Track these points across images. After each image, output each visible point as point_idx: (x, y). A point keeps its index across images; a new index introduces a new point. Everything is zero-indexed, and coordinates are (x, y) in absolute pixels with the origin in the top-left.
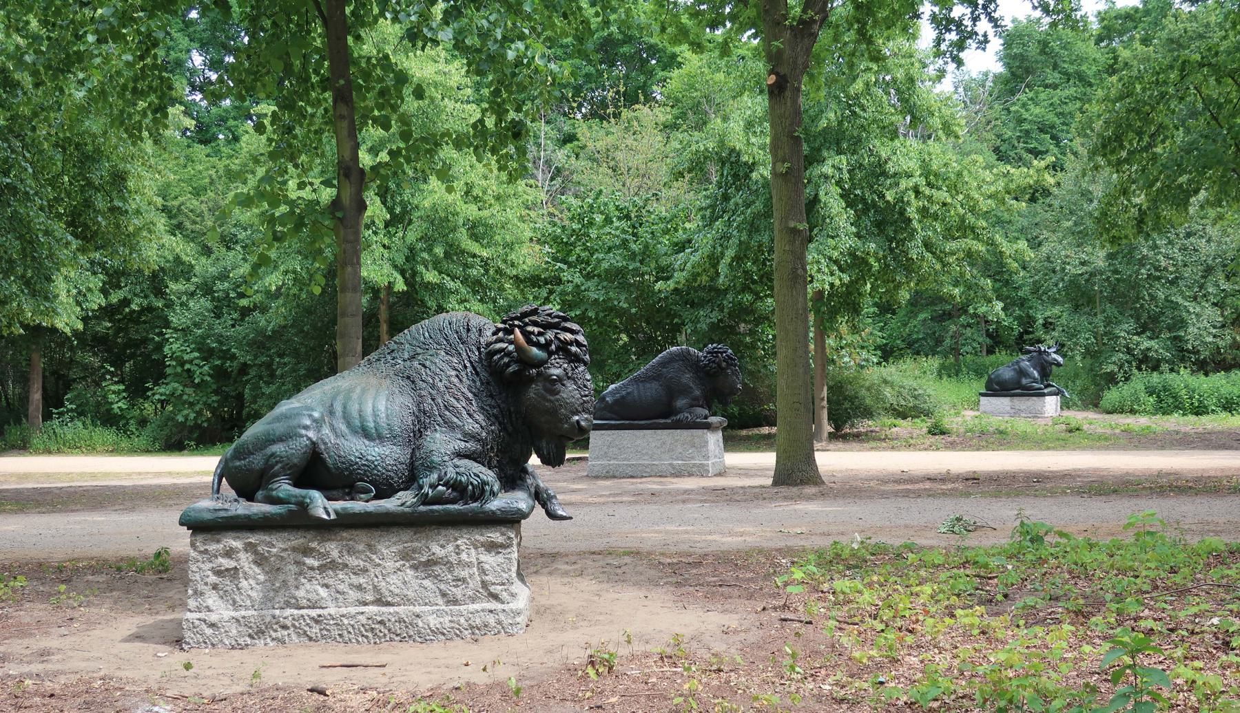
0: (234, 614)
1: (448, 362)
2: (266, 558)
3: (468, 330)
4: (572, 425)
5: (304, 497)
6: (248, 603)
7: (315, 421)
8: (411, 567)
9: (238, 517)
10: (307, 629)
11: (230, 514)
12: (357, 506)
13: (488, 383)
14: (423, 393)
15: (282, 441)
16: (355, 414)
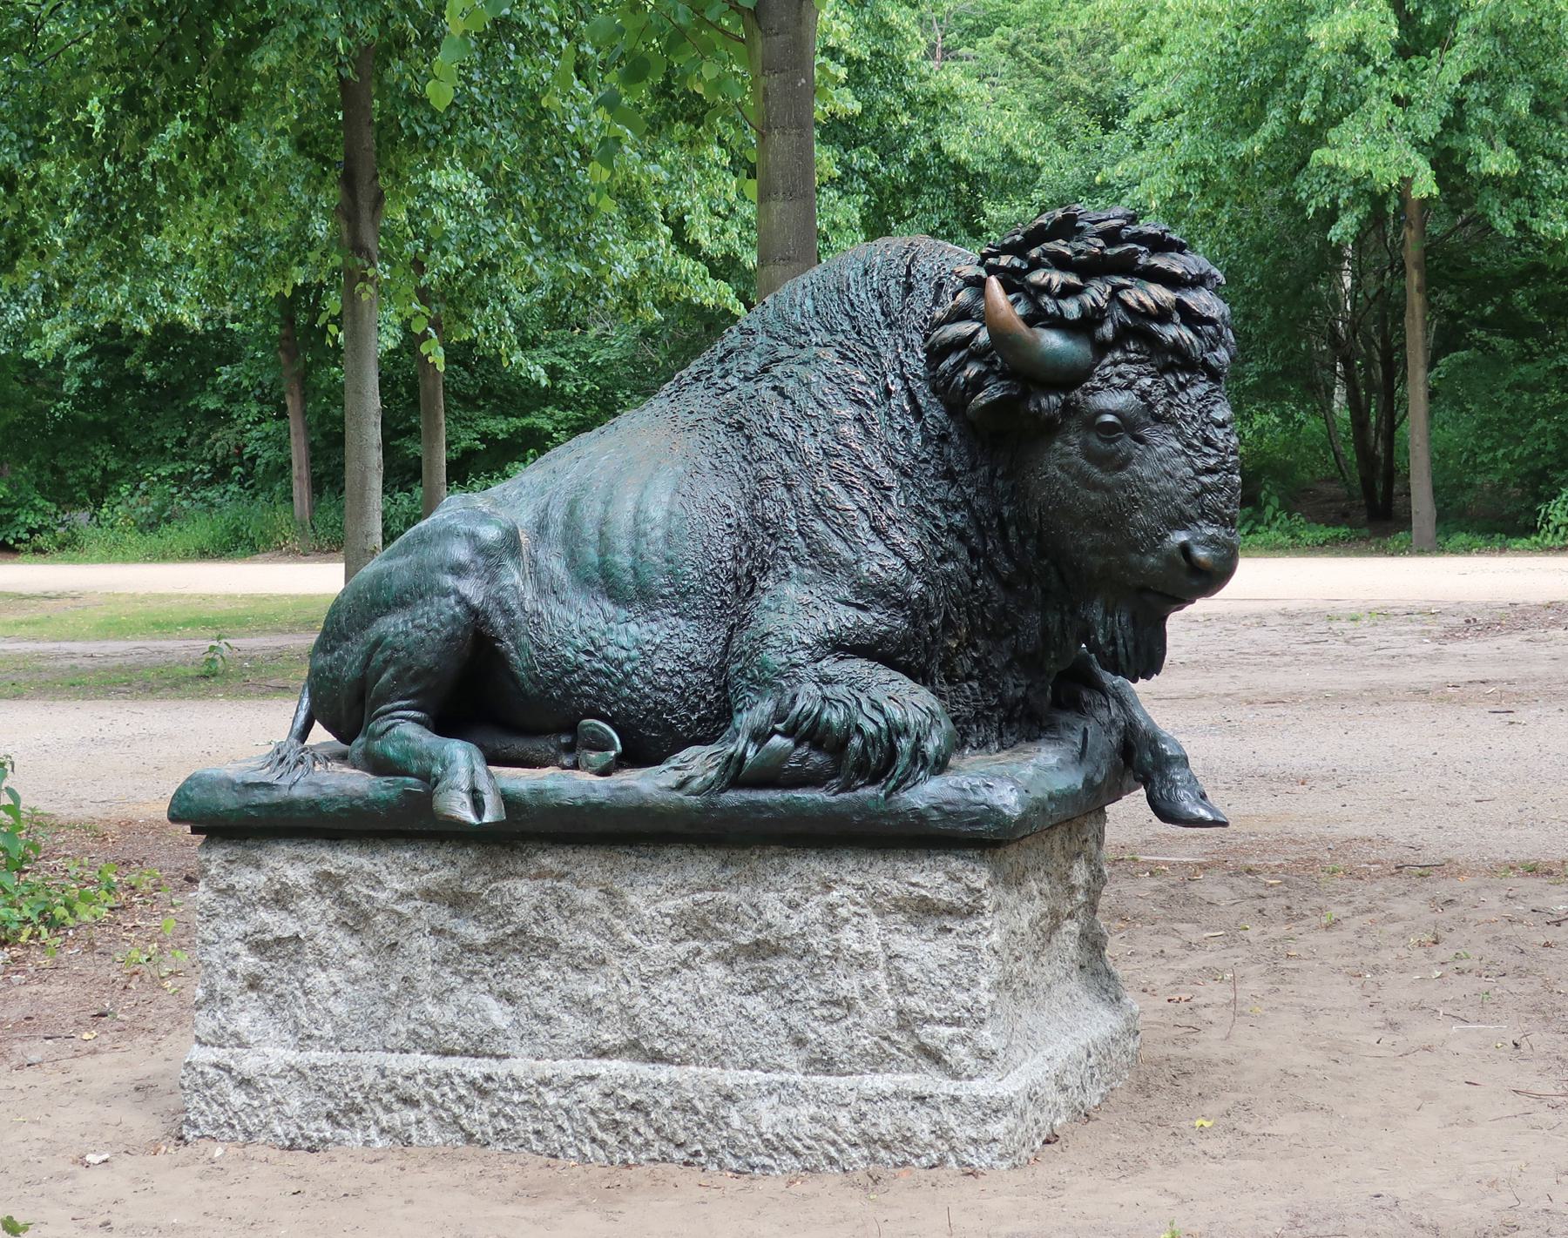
0: (292, 1056)
1: (839, 381)
2: (366, 917)
3: (909, 289)
4: (1169, 560)
6: (328, 1030)
7: (483, 550)
8: (717, 957)
9: (291, 805)
10: (459, 1109)
11: (276, 796)
13: (943, 438)
15: (403, 604)
16: (590, 531)
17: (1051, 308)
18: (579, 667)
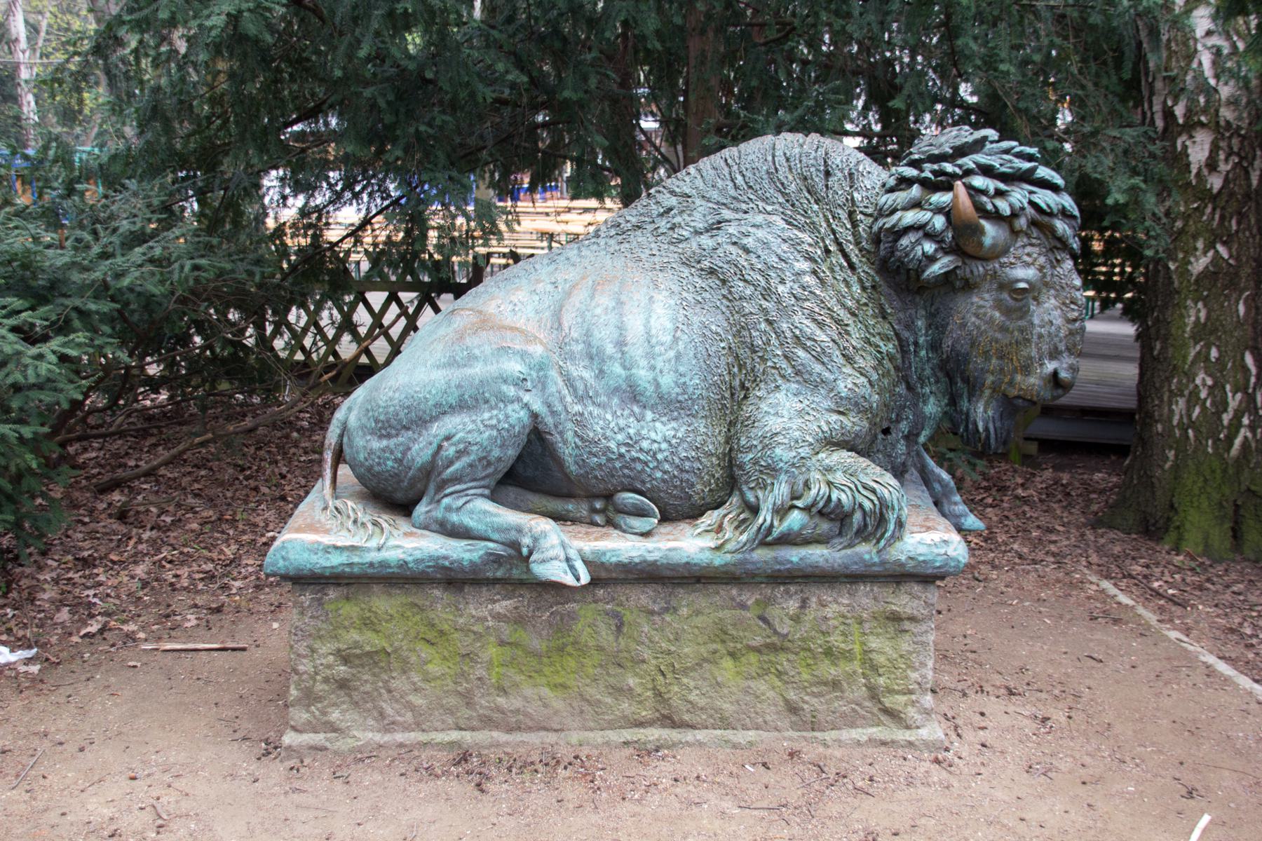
1: (795, 244)
3: (828, 174)
5: (519, 530)
9: (384, 564)
12: (622, 546)
14: (748, 307)
17: (989, 207)
18: (621, 456)
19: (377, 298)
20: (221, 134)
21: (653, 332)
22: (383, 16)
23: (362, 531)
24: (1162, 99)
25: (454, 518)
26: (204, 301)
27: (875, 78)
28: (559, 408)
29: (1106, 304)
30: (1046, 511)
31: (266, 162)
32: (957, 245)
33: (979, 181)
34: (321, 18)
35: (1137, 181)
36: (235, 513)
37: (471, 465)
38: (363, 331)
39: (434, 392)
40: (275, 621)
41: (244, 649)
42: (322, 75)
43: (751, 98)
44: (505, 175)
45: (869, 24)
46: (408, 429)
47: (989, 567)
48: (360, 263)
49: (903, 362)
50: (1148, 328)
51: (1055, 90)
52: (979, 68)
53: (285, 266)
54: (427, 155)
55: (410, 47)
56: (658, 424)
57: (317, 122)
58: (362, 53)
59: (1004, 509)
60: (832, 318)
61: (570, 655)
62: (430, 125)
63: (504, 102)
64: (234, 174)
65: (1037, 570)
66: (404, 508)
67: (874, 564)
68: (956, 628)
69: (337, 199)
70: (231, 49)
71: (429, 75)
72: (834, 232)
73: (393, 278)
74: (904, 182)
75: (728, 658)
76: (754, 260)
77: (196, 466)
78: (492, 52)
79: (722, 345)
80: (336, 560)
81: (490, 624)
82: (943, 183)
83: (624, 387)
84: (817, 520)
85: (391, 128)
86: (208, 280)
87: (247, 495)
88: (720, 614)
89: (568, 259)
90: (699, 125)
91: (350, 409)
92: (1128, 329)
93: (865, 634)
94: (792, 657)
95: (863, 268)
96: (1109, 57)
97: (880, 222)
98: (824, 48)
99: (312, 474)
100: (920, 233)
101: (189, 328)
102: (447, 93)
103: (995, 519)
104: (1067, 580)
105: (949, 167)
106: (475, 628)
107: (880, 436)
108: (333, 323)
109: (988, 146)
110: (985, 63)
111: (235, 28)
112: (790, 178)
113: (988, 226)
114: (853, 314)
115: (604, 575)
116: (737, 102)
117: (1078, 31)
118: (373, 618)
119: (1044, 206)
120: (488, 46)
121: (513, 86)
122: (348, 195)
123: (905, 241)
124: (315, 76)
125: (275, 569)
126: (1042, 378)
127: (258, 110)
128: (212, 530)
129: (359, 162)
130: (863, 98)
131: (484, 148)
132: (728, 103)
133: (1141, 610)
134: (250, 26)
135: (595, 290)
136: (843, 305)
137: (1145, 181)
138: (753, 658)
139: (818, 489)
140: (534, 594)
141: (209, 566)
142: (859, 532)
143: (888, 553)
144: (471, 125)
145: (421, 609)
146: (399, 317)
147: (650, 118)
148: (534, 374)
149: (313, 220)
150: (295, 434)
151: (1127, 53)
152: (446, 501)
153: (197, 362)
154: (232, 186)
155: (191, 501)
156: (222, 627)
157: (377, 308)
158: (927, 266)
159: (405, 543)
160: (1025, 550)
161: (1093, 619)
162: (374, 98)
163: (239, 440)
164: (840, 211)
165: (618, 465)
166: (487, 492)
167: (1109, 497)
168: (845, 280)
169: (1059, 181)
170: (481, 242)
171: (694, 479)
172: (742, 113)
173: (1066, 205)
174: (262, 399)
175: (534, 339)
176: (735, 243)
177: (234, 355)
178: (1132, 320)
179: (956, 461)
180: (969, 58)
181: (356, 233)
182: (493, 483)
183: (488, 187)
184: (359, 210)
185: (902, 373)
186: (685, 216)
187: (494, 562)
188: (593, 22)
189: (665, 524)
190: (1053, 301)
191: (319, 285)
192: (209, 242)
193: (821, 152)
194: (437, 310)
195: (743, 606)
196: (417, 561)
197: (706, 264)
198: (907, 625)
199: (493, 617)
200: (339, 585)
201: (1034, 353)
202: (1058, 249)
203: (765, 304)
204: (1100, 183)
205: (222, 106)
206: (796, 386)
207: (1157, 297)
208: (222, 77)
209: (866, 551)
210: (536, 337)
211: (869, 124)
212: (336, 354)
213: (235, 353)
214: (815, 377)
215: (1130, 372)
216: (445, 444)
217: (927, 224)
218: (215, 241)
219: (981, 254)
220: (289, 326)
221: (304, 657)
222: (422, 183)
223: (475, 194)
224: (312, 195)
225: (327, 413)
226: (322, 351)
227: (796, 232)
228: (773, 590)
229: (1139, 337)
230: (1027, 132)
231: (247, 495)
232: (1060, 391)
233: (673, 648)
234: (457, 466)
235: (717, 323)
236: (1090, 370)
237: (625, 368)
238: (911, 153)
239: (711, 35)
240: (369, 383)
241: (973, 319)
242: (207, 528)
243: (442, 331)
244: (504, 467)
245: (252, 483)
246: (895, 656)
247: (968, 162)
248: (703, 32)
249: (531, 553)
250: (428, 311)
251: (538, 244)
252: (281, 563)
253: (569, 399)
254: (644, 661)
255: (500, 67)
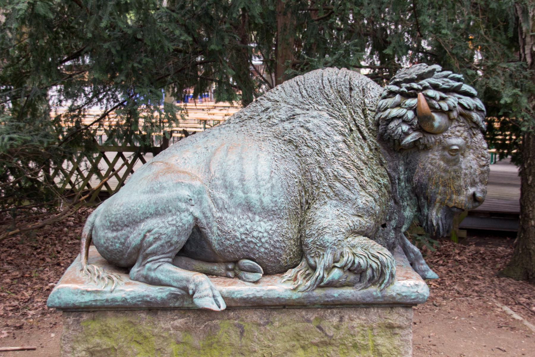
1: (334, 126)
3: (351, 89)
9: (114, 300)
12: (243, 289)
14: (309, 160)
17: (437, 106)
18: (242, 240)
19: (111, 155)
20: (25, 66)
21: (259, 174)
22: (114, 5)
23: (102, 282)
24: (530, 47)
25: (152, 274)
26: (16, 157)
27: (376, 38)
28: (209, 214)
29: (502, 156)
30: (472, 268)
31: (50, 82)
32: (420, 126)
33: (431, 93)
34: (80, 5)
35: (517, 91)
36: (31, 273)
37: (162, 246)
38: (103, 173)
39: (142, 206)
40: (53, 332)
41: (34, 349)
42: (81, 35)
43: (311, 48)
44: (180, 89)
45: (373, 9)
46: (128, 226)
47: (441, 298)
48: (102, 136)
49: (392, 189)
50: (525, 169)
51: (472, 43)
52: (431, 32)
53: (61, 137)
54: (138, 79)
55: (129, 22)
56: (262, 223)
57: (78, 60)
58: (103, 25)
59: (449, 267)
60: (354, 165)
61: (215, 348)
62: (139, 63)
63: (180, 51)
64: (32, 88)
65: (468, 300)
66: (126, 269)
67: (379, 298)
68: (425, 332)
69: (89, 102)
70: (30, 21)
71: (139, 36)
72: (355, 120)
73: (120, 145)
74: (392, 94)
75: (301, 349)
76: (313, 135)
77: (9, 247)
78: (173, 25)
79: (296, 180)
80: (87, 298)
81: (172, 332)
82: (412, 94)
83: (244, 203)
84: (347, 273)
85: (120, 63)
86: (18, 146)
87: (38, 263)
88: (296, 325)
89: (214, 135)
90: (283, 63)
91: (96, 216)
92: (514, 169)
93: (374, 336)
94: (335, 348)
95: (371, 139)
96: (501, 25)
97: (379, 115)
98: (349, 22)
99: (75, 251)
100: (401, 120)
101: (7, 172)
102: (149, 46)
103: (444, 272)
104: (484, 305)
105: (415, 85)
106: (164, 335)
107: (381, 228)
108: (87, 169)
109: (436, 74)
110: (435, 29)
111: (33, 9)
112: (331, 91)
113: (436, 116)
114: (365, 164)
115: (233, 304)
116: (303, 50)
117: (484, 11)
118: (107, 330)
119: (466, 106)
120: (170, 21)
121: (184, 42)
122: (95, 100)
123: (392, 125)
124: (77, 36)
125: (53, 304)
126: (467, 197)
127: (46, 54)
128: (18, 283)
129: (101, 82)
130: (370, 48)
131: (169, 75)
132: (299, 51)
133: (526, 323)
134: (41, 9)
135: (228, 151)
136: (360, 159)
137: (521, 91)
138: (314, 349)
139: (348, 258)
140: (196, 316)
141: (16, 303)
142: (370, 280)
143: (386, 291)
144: (162, 63)
145: (134, 325)
146: (123, 165)
147: (257, 59)
148: (196, 197)
149: (76, 113)
150: (66, 229)
151: (511, 23)
152: (148, 265)
153: (11, 190)
154: (31, 95)
155: (6, 266)
156: (22, 337)
157: (111, 160)
158: (404, 138)
159: (126, 288)
160: (461, 289)
161: (500, 327)
162: (109, 48)
163: (35, 232)
164: (358, 109)
165: (241, 245)
166: (170, 260)
167: (506, 260)
168: (361, 145)
169: (474, 92)
170: (167, 125)
171: (281, 252)
172: (306, 57)
173: (478, 104)
174: (48, 210)
175: (195, 178)
176: (302, 126)
177: (32, 187)
178: (516, 165)
179: (422, 241)
180: (426, 27)
181: (100, 120)
182: (174, 255)
183: (171, 96)
184: (102, 108)
185: (392, 194)
186: (276, 112)
187: (174, 298)
188: (226, 9)
189: (266, 277)
190: (472, 156)
191: (80, 148)
192: (19, 125)
193: (348, 78)
194: (144, 162)
195: (308, 321)
196: (132, 298)
197: (287, 137)
198: (397, 331)
199: (174, 328)
200: (89, 312)
201: (462, 183)
202: (474, 128)
203: (318, 158)
204: (498, 92)
205: (26, 51)
206: (335, 202)
207: (529, 152)
208: (25, 36)
209: (374, 290)
210: (197, 177)
211: (374, 61)
212: (88, 185)
213: (33, 185)
214: (345, 197)
215: (516, 192)
216: (148, 234)
217: (404, 115)
218: (22, 125)
219: (433, 131)
220: (63, 171)
221: (69, 352)
222: (135, 94)
223: (164, 99)
224: (76, 100)
225: (84, 217)
226: (81, 184)
227: (335, 120)
228: (324, 312)
229: (520, 174)
230: (457, 65)
231: (38, 263)
232: (477, 204)
233: (271, 344)
234: (154, 246)
235: (293, 168)
236: (493, 191)
237: (244, 193)
238: (395, 78)
239: (289, 15)
240: (107, 201)
241: (429, 166)
242: (15, 282)
243: (146, 174)
244: (179, 247)
245: (41, 256)
246: (391, 347)
247: (425, 82)
248: (285, 14)
249: (194, 293)
250: (139, 162)
251: (199, 126)
252: (57, 301)
253: (214, 210)
254: (255, 352)
255: (177, 32)
